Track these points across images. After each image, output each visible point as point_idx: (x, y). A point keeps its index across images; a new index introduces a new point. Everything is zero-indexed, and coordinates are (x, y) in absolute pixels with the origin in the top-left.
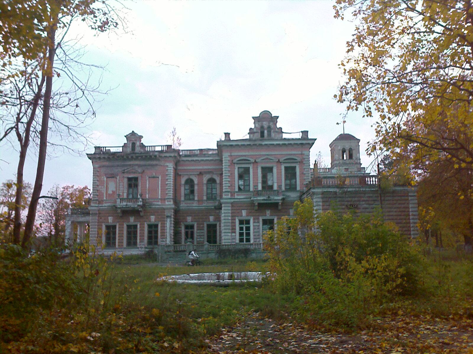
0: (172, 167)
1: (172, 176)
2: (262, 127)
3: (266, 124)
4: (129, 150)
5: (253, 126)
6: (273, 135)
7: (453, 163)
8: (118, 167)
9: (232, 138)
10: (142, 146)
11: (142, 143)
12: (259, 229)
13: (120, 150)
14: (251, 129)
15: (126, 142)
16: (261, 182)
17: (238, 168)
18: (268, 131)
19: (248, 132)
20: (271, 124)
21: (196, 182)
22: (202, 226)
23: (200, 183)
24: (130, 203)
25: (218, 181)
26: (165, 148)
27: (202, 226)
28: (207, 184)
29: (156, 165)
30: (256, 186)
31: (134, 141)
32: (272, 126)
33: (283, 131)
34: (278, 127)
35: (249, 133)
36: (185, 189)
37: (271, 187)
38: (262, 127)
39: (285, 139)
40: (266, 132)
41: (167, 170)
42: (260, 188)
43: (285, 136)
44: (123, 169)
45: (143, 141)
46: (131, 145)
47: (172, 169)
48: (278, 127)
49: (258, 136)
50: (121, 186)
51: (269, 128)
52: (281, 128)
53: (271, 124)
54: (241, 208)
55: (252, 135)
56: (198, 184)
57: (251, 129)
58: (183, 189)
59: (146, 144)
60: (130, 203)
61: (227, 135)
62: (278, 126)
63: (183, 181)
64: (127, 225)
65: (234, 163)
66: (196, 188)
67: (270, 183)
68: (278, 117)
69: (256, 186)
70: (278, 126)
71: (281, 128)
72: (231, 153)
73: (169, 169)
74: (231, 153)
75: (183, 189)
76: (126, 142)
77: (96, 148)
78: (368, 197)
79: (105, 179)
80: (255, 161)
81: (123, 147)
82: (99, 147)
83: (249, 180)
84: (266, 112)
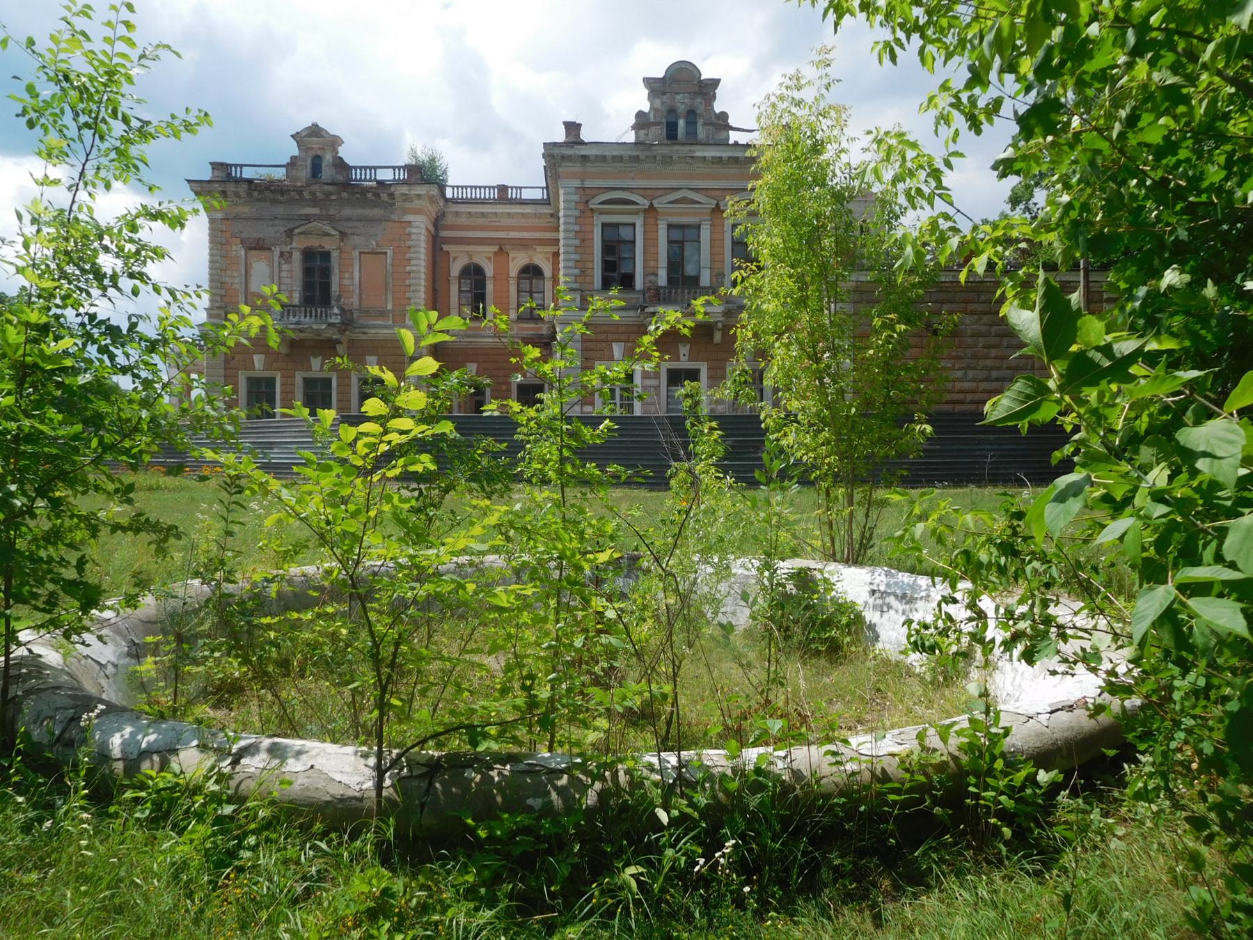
0: (422, 225)
1: (423, 251)
2: (672, 111)
3: (683, 103)
4: (304, 173)
5: (646, 107)
6: (702, 133)
7: (1169, 181)
8: (276, 222)
9: (586, 135)
10: (341, 165)
11: (341, 158)
12: (658, 395)
13: (280, 174)
14: (640, 115)
15: (297, 153)
16: (665, 265)
17: (604, 225)
18: (687, 123)
19: (633, 121)
20: (699, 104)
21: (489, 271)
22: (504, 388)
23: (501, 276)
24: (308, 319)
25: (548, 273)
26: (403, 175)
27: (504, 388)
28: (519, 278)
29: (381, 220)
30: (650, 273)
31: (319, 153)
32: (701, 109)
33: (731, 122)
34: (718, 109)
35: (633, 128)
36: (460, 291)
37: (695, 280)
38: (672, 111)
39: (736, 144)
40: (681, 123)
41: (409, 234)
42: (662, 280)
43: (734, 137)
44: (290, 226)
45: (343, 152)
46: (309, 161)
47: (423, 231)
48: (718, 109)
49: (656, 133)
50: (284, 274)
51: (691, 114)
52: (724, 116)
53: (699, 104)
54: (610, 337)
55: (642, 132)
56: (494, 278)
57: (640, 115)
58: (454, 289)
59: (350, 161)
60: (308, 319)
61: (572, 128)
62: (718, 108)
63: (455, 271)
64: (305, 379)
65: (592, 210)
66: (489, 287)
67: (690, 270)
68: (718, 81)
69: (650, 273)
70: (718, 108)
71: (724, 116)
72: (583, 181)
73: (414, 230)
74: (583, 181)
75: (454, 289)
76: (296, 152)
77: (216, 166)
78: (997, 335)
79: (243, 252)
80: (651, 205)
81: (287, 166)
82: (222, 164)
83: (634, 258)
84: (683, 66)
